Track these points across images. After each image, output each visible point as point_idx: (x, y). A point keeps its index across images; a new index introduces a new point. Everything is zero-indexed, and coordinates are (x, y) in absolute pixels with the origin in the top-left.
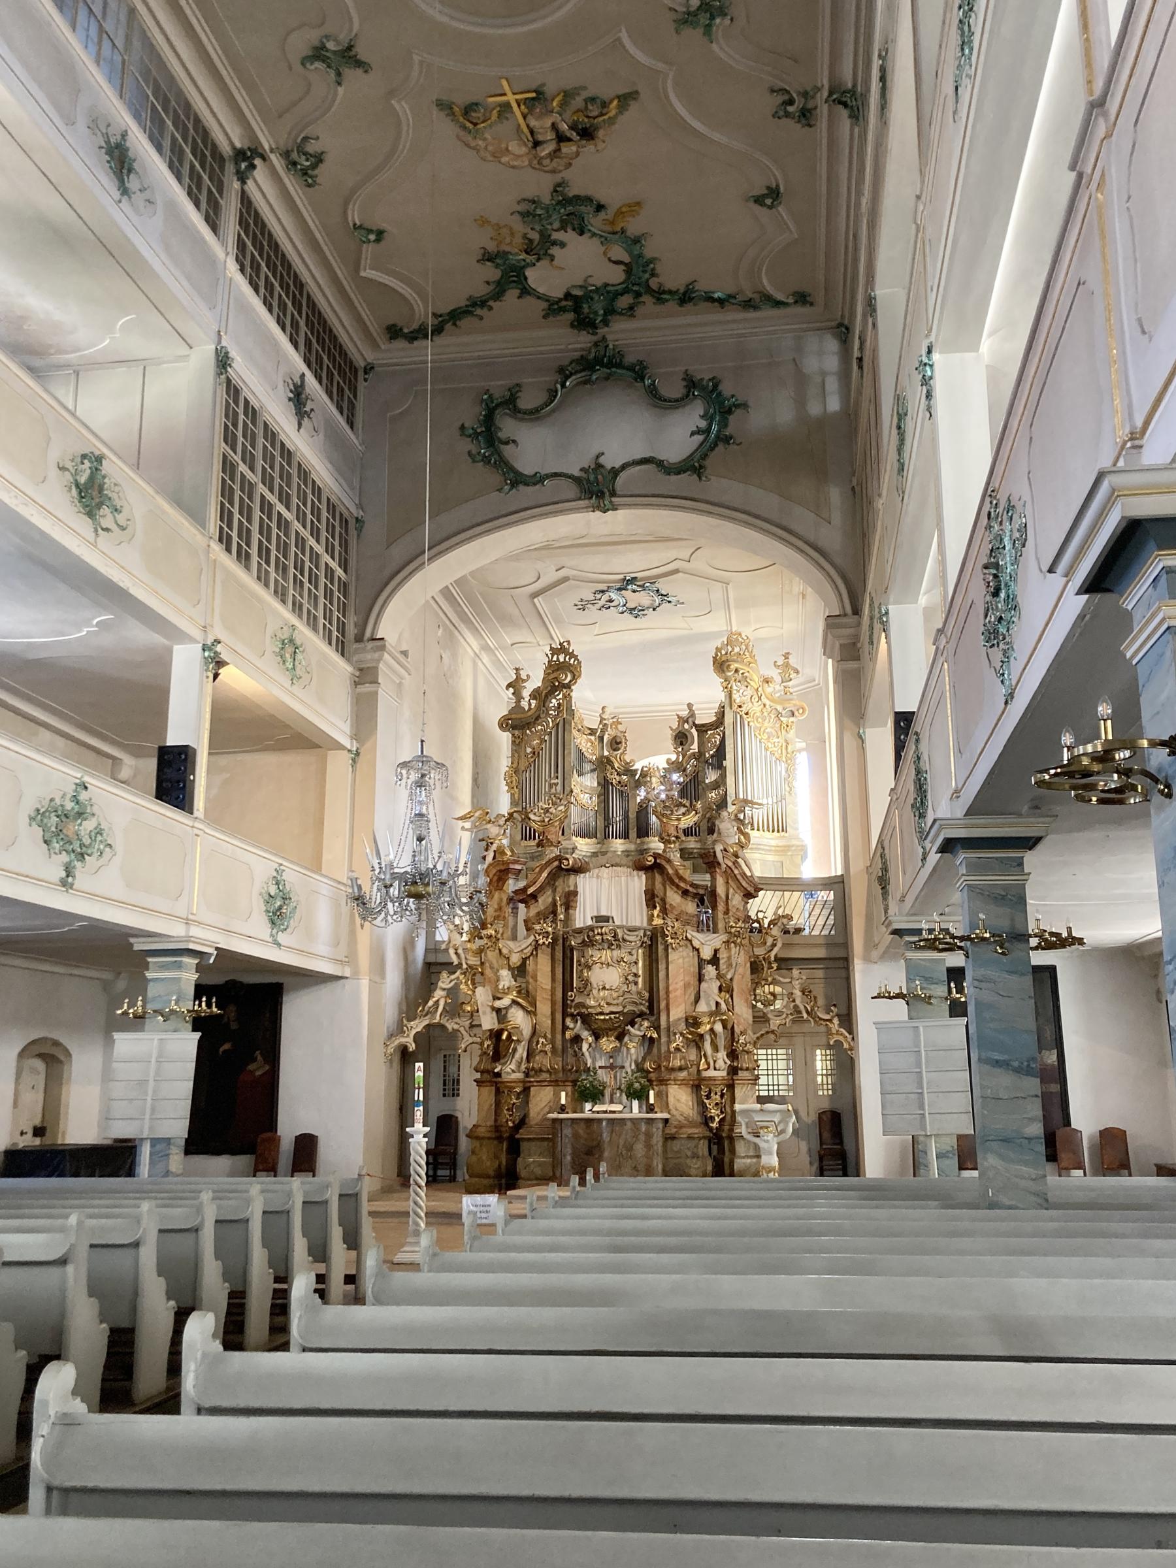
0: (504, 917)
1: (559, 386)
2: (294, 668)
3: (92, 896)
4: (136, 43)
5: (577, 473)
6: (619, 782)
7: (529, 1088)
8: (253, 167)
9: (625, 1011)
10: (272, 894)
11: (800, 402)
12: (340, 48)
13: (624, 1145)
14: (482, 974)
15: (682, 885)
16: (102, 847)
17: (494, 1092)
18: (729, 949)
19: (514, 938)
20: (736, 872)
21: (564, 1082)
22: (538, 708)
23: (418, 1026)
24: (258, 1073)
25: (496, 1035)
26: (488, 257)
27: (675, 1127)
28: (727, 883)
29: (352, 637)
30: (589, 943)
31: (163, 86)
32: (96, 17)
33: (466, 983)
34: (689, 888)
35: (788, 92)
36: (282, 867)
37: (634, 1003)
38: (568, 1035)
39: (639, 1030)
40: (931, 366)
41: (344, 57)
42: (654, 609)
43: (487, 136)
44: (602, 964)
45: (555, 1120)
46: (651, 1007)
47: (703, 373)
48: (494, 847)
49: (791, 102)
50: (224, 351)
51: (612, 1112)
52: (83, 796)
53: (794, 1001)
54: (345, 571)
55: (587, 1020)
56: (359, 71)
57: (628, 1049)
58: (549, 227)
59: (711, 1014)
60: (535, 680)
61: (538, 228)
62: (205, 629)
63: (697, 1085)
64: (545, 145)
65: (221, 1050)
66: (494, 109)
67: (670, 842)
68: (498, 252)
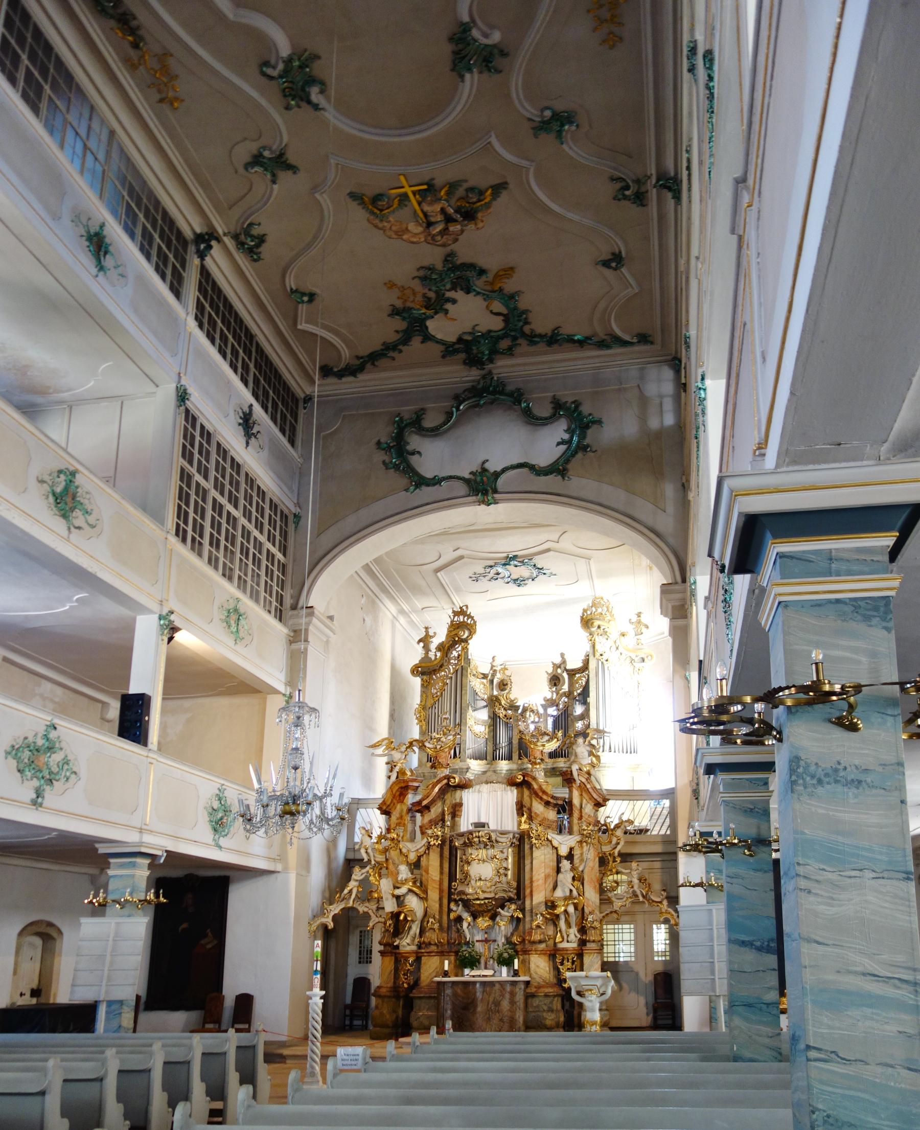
0: (404, 824)
1: (454, 409)
2: (237, 631)
3: (59, 812)
4: (115, 155)
5: (467, 476)
6: (505, 716)
7: (421, 957)
8: (210, 247)
9: (497, 897)
10: (215, 807)
11: (643, 418)
12: (274, 156)
13: (494, 1002)
14: (387, 868)
15: (545, 797)
16: (68, 774)
17: (393, 961)
18: (582, 847)
19: (413, 839)
20: (588, 786)
21: (448, 952)
22: (442, 658)
23: (336, 909)
24: (209, 946)
25: (395, 916)
26: (395, 312)
27: (535, 987)
28: (581, 795)
29: (289, 606)
30: (469, 844)
31: (137, 188)
32: (81, 137)
34: (550, 799)
35: (624, 180)
36: (224, 787)
37: (504, 891)
38: (452, 916)
39: (508, 912)
40: (705, 390)
41: (277, 162)
42: (533, 580)
43: (391, 219)
44: (479, 860)
45: (439, 983)
47: (567, 397)
48: (397, 769)
49: (627, 187)
50: (182, 388)
51: (484, 976)
52: (53, 735)
53: (632, 887)
54: (284, 555)
55: (467, 904)
56: (290, 173)
57: (500, 926)
58: (443, 288)
59: (565, 899)
60: (440, 636)
61: (434, 288)
62: (161, 603)
63: (554, 954)
64: (437, 225)
65: (180, 928)
66: (396, 198)
67: (535, 763)
68: (404, 308)
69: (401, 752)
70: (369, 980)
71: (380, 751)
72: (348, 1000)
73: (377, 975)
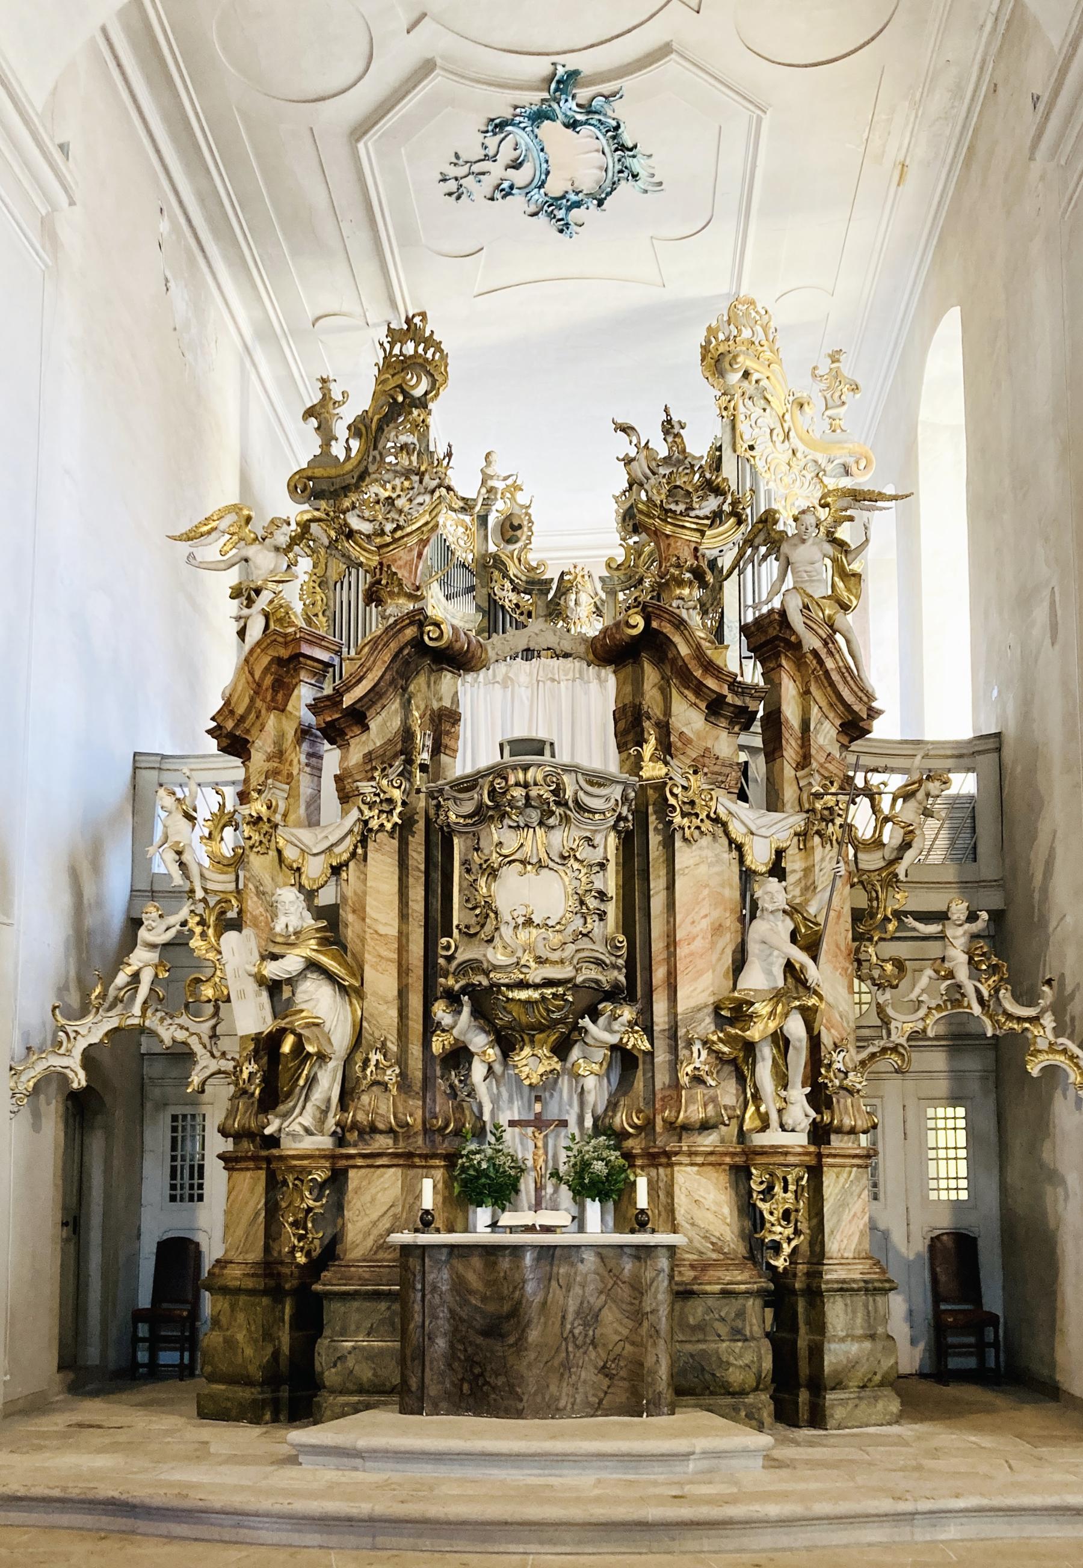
0: (290, 775)
6: (517, 606)
7: (344, 1172)
9: (579, 979)
15: (711, 683)
19: (313, 821)
20: (830, 664)
21: (426, 1157)
22: (364, 453)
27: (692, 1267)
28: (807, 692)
33: (203, 935)
37: (599, 963)
39: (609, 1029)
44: (524, 862)
46: (631, 976)
59: (778, 996)
69: (277, 549)
70: (197, 1244)
71: (211, 551)
72: (145, 1300)
73: (218, 1233)
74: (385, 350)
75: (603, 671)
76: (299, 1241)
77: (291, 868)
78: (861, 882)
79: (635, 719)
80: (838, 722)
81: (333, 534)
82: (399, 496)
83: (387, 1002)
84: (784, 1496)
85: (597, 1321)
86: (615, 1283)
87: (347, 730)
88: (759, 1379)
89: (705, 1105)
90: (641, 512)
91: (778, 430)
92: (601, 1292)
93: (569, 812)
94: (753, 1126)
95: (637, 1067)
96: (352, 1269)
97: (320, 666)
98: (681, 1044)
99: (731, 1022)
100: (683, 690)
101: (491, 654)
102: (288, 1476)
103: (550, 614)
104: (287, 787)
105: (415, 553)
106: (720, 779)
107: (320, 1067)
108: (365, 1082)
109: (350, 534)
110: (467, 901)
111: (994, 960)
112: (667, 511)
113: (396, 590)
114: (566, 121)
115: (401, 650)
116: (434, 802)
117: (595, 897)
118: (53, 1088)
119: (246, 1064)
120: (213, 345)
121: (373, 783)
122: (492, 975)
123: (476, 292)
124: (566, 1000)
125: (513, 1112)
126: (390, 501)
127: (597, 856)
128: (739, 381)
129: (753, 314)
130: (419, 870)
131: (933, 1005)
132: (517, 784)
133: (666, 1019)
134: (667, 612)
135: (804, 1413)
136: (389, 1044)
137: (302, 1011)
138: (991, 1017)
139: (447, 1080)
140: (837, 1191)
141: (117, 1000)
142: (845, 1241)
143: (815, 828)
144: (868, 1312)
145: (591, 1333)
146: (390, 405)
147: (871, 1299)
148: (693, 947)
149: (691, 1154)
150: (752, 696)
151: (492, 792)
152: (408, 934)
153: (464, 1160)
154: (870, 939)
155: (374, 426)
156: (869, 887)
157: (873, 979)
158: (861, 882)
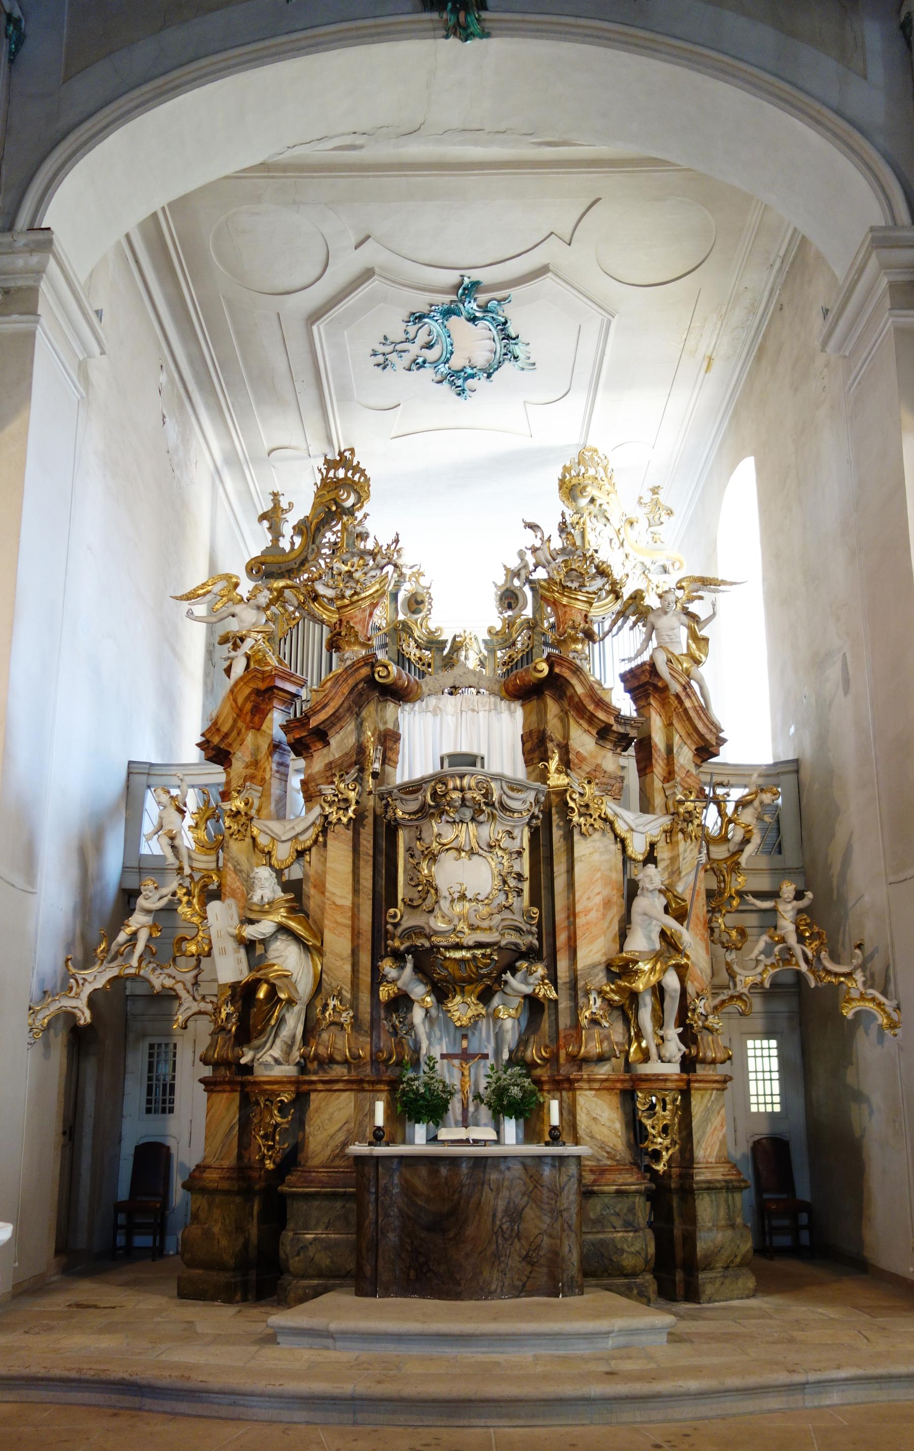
0: (263, 780)
6: (420, 659)
7: (307, 1094)
9: (503, 943)
13: (506, 1211)
15: (601, 715)
19: (280, 816)
20: (688, 704)
21: (373, 1083)
22: (304, 546)
27: (592, 1171)
33: (189, 903)
37: (518, 930)
38: (384, 993)
39: (525, 982)
44: (459, 850)
45: (360, 1160)
59: (657, 956)
69: (258, 608)
70: (168, 1148)
72: (123, 1192)
74: (322, 474)
75: (513, 705)
76: (268, 1151)
77: (263, 852)
78: (712, 869)
79: (540, 741)
80: (694, 747)
81: (302, 598)
82: (357, 570)
83: (342, 959)
84: (696, 1371)
85: (521, 1218)
86: (535, 1187)
87: (311, 745)
88: (647, 1262)
89: (601, 1042)
90: (542, 587)
91: (615, 540)
92: (524, 1194)
93: (495, 811)
94: (636, 1058)
95: (544, 1011)
96: (314, 1174)
97: (289, 696)
98: (580, 993)
99: (619, 976)
100: (578, 719)
101: (425, 689)
102: (270, 1356)
103: (445, 666)
104: (261, 788)
105: (368, 613)
106: (609, 788)
107: (288, 1010)
108: (324, 1023)
109: (316, 598)
110: (411, 879)
111: (816, 929)
112: (564, 587)
113: (353, 640)
114: (468, 316)
115: (357, 685)
116: (384, 802)
117: (514, 878)
118: (61, 1023)
119: (224, 1007)
120: (194, 465)
121: (333, 786)
122: (433, 939)
123: (393, 435)
124: (493, 959)
125: (442, 1048)
126: (350, 574)
127: (515, 846)
128: (588, 504)
129: (596, 459)
130: (368, 855)
131: (769, 963)
132: (455, 789)
133: (567, 974)
134: (566, 660)
135: (680, 1289)
136: (344, 992)
137: (274, 965)
138: (813, 973)
139: (390, 1021)
140: (701, 1109)
141: (118, 954)
142: (709, 1150)
143: (679, 827)
144: (728, 1206)
145: (516, 1227)
146: (326, 512)
147: (730, 1195)
148: (589, 917)
149: (590, 1081)
150: (632, 726)
151: (434, 795)
152: (359, 905)
153: (405, 1085)
154: (720, 911)
155: (313, 527)
156: (718, 873)
157: (722, 943)
158: (712, 869)
